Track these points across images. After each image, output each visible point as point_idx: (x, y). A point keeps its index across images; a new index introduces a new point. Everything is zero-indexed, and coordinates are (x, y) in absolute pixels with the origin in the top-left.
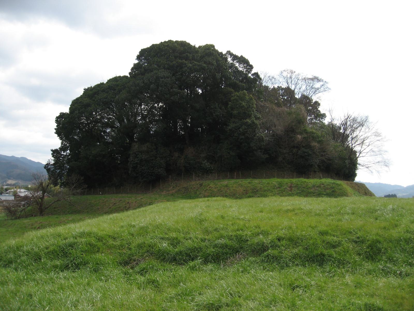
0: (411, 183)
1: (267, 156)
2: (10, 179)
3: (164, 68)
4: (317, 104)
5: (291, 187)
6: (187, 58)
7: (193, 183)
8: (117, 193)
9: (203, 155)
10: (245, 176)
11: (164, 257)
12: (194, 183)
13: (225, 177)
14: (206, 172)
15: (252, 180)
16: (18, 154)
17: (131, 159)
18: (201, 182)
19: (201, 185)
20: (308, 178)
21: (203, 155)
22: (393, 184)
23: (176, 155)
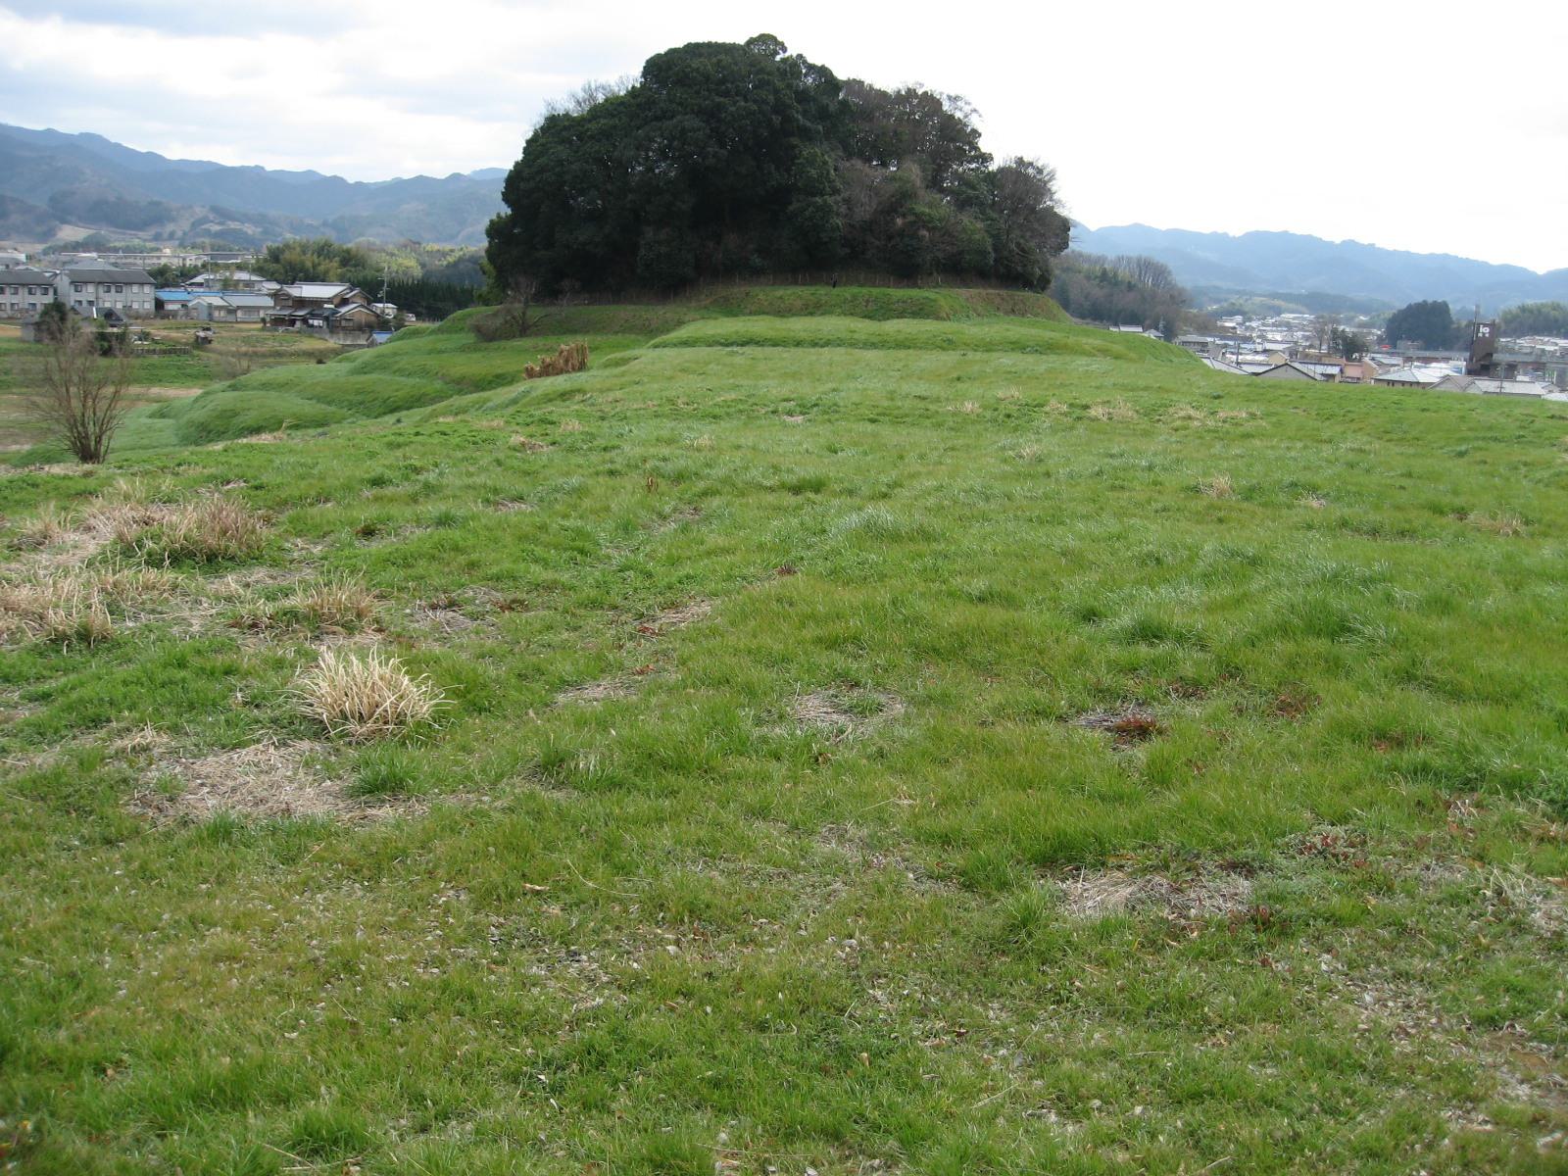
0: (1562, 265)
1: (848, 251)
2: (68, 223)
3: (693, 111)
4: (976, 133)
5: (868, 301)
6: (726, 94)
7: (736, 290)
8: (614, 302)
9: (751, 246)
10: (814, 281)
11: (722, 344)
12: (737, 290)
13: (785, 282)
14: (755, 274)
15: (625, 361)
16: (71, 121)
17: (643, 252)
18: (748, 289)
19: (747, 294)
20: (915, 285)
21: (751, 246)
22: (1495, 258)
23: (711, 244)
